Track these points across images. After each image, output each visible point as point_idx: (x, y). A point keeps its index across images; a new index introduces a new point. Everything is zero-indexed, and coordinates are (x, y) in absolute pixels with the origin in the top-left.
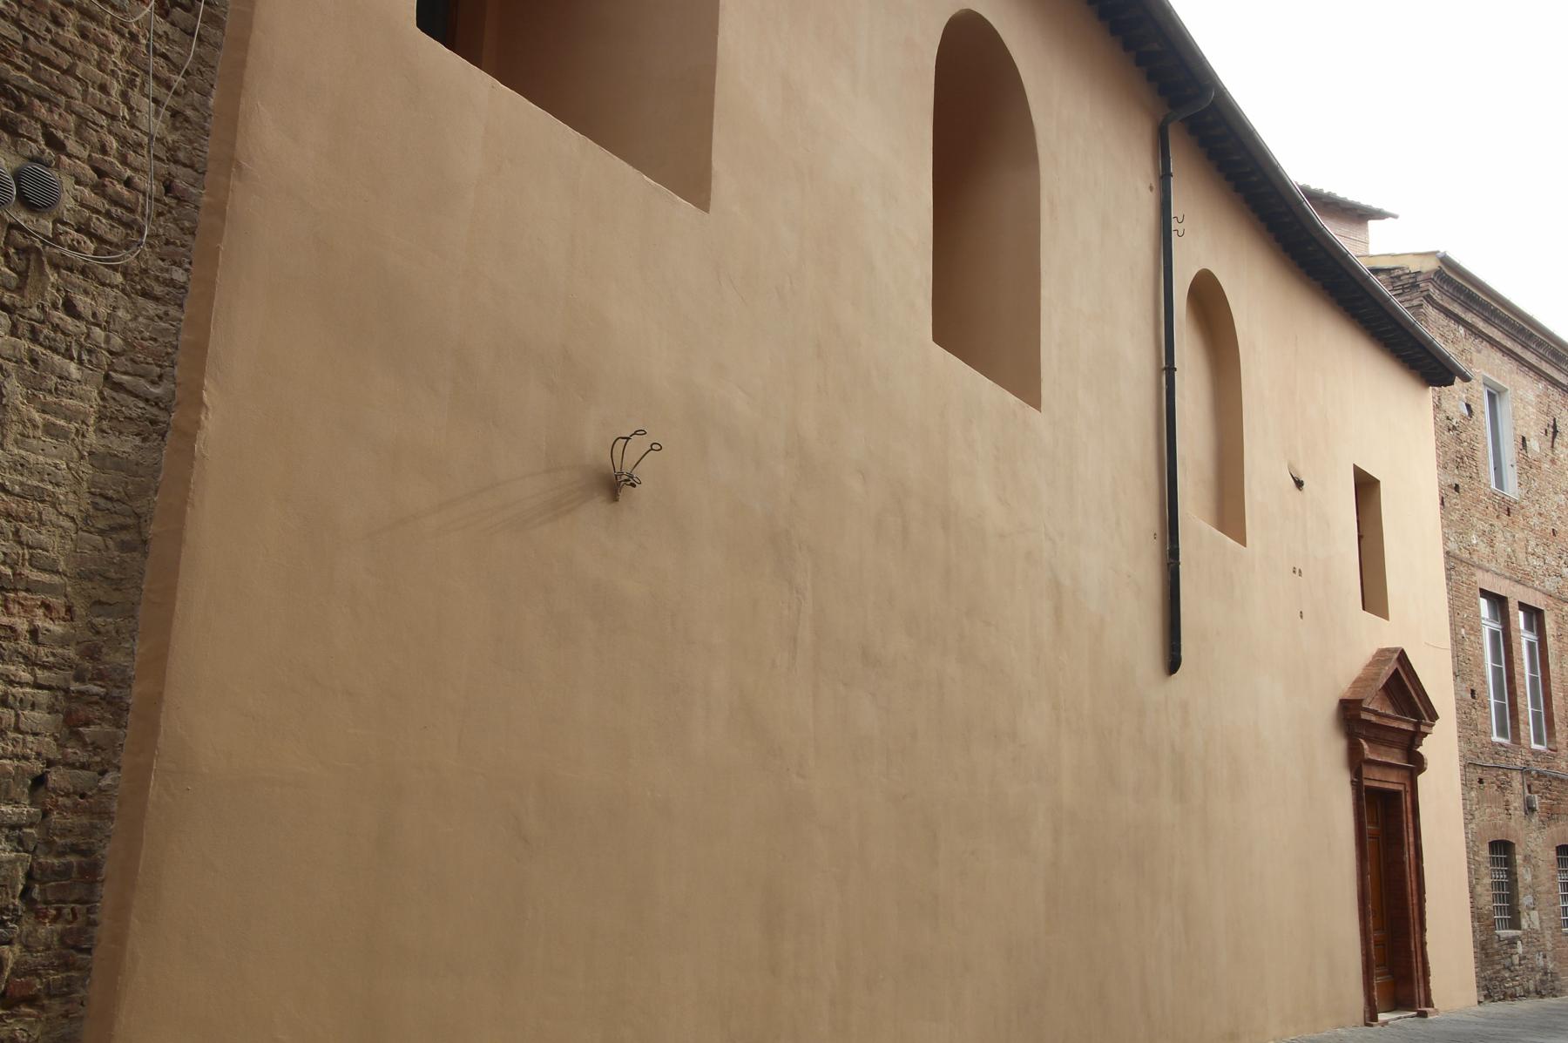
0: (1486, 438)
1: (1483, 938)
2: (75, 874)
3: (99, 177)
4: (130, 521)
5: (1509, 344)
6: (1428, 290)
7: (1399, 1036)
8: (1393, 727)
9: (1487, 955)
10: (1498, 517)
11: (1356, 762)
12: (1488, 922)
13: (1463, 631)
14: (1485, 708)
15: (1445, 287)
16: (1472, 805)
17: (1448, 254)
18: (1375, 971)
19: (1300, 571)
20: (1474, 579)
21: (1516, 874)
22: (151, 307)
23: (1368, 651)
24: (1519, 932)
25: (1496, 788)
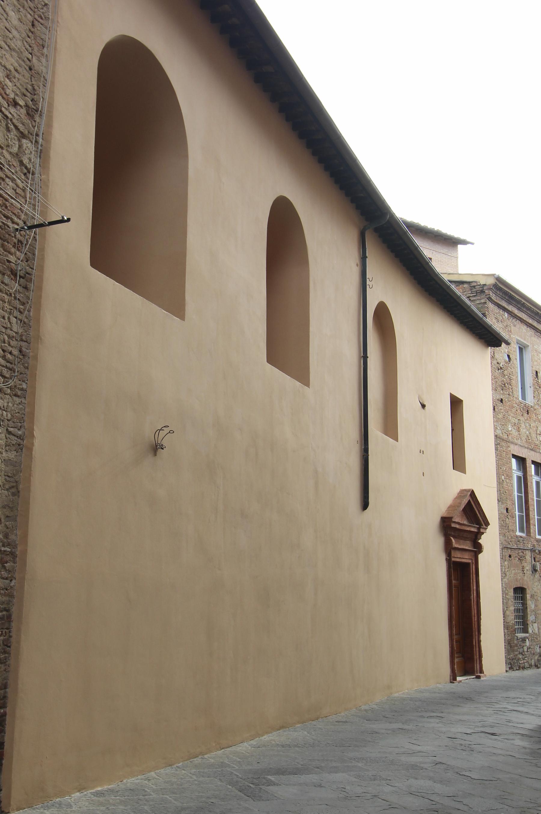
0: (517, 373)
1: (509, 638)
2: (5, 618)
3: (4, 352)
4: (14, 484)
5: (530, 321)
6: (489, 294)
7: (467, 687)
8: (467, 530)
9: (511, 647)
10: (522, 415)
11: (448, 549)
12: (512, 630)
13: (503, 477)
14: (513, 517)
15: (498, 292)
16: (505, 569)
17: (500, 276)
18: (456, 656)
19: (423, 451)
20: (509, 449)
21: (527, 604)
22: (17, 400)
23: (454, 492)
24: (527, 635)
25: (518, 559)
